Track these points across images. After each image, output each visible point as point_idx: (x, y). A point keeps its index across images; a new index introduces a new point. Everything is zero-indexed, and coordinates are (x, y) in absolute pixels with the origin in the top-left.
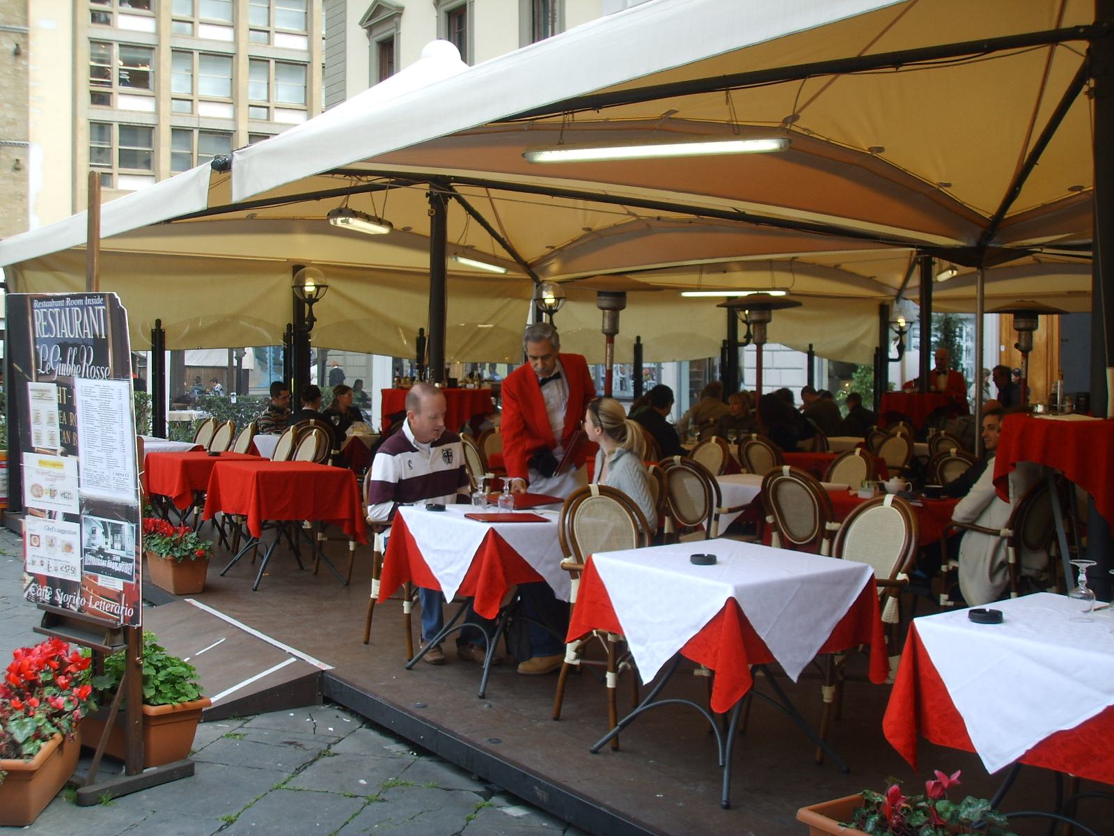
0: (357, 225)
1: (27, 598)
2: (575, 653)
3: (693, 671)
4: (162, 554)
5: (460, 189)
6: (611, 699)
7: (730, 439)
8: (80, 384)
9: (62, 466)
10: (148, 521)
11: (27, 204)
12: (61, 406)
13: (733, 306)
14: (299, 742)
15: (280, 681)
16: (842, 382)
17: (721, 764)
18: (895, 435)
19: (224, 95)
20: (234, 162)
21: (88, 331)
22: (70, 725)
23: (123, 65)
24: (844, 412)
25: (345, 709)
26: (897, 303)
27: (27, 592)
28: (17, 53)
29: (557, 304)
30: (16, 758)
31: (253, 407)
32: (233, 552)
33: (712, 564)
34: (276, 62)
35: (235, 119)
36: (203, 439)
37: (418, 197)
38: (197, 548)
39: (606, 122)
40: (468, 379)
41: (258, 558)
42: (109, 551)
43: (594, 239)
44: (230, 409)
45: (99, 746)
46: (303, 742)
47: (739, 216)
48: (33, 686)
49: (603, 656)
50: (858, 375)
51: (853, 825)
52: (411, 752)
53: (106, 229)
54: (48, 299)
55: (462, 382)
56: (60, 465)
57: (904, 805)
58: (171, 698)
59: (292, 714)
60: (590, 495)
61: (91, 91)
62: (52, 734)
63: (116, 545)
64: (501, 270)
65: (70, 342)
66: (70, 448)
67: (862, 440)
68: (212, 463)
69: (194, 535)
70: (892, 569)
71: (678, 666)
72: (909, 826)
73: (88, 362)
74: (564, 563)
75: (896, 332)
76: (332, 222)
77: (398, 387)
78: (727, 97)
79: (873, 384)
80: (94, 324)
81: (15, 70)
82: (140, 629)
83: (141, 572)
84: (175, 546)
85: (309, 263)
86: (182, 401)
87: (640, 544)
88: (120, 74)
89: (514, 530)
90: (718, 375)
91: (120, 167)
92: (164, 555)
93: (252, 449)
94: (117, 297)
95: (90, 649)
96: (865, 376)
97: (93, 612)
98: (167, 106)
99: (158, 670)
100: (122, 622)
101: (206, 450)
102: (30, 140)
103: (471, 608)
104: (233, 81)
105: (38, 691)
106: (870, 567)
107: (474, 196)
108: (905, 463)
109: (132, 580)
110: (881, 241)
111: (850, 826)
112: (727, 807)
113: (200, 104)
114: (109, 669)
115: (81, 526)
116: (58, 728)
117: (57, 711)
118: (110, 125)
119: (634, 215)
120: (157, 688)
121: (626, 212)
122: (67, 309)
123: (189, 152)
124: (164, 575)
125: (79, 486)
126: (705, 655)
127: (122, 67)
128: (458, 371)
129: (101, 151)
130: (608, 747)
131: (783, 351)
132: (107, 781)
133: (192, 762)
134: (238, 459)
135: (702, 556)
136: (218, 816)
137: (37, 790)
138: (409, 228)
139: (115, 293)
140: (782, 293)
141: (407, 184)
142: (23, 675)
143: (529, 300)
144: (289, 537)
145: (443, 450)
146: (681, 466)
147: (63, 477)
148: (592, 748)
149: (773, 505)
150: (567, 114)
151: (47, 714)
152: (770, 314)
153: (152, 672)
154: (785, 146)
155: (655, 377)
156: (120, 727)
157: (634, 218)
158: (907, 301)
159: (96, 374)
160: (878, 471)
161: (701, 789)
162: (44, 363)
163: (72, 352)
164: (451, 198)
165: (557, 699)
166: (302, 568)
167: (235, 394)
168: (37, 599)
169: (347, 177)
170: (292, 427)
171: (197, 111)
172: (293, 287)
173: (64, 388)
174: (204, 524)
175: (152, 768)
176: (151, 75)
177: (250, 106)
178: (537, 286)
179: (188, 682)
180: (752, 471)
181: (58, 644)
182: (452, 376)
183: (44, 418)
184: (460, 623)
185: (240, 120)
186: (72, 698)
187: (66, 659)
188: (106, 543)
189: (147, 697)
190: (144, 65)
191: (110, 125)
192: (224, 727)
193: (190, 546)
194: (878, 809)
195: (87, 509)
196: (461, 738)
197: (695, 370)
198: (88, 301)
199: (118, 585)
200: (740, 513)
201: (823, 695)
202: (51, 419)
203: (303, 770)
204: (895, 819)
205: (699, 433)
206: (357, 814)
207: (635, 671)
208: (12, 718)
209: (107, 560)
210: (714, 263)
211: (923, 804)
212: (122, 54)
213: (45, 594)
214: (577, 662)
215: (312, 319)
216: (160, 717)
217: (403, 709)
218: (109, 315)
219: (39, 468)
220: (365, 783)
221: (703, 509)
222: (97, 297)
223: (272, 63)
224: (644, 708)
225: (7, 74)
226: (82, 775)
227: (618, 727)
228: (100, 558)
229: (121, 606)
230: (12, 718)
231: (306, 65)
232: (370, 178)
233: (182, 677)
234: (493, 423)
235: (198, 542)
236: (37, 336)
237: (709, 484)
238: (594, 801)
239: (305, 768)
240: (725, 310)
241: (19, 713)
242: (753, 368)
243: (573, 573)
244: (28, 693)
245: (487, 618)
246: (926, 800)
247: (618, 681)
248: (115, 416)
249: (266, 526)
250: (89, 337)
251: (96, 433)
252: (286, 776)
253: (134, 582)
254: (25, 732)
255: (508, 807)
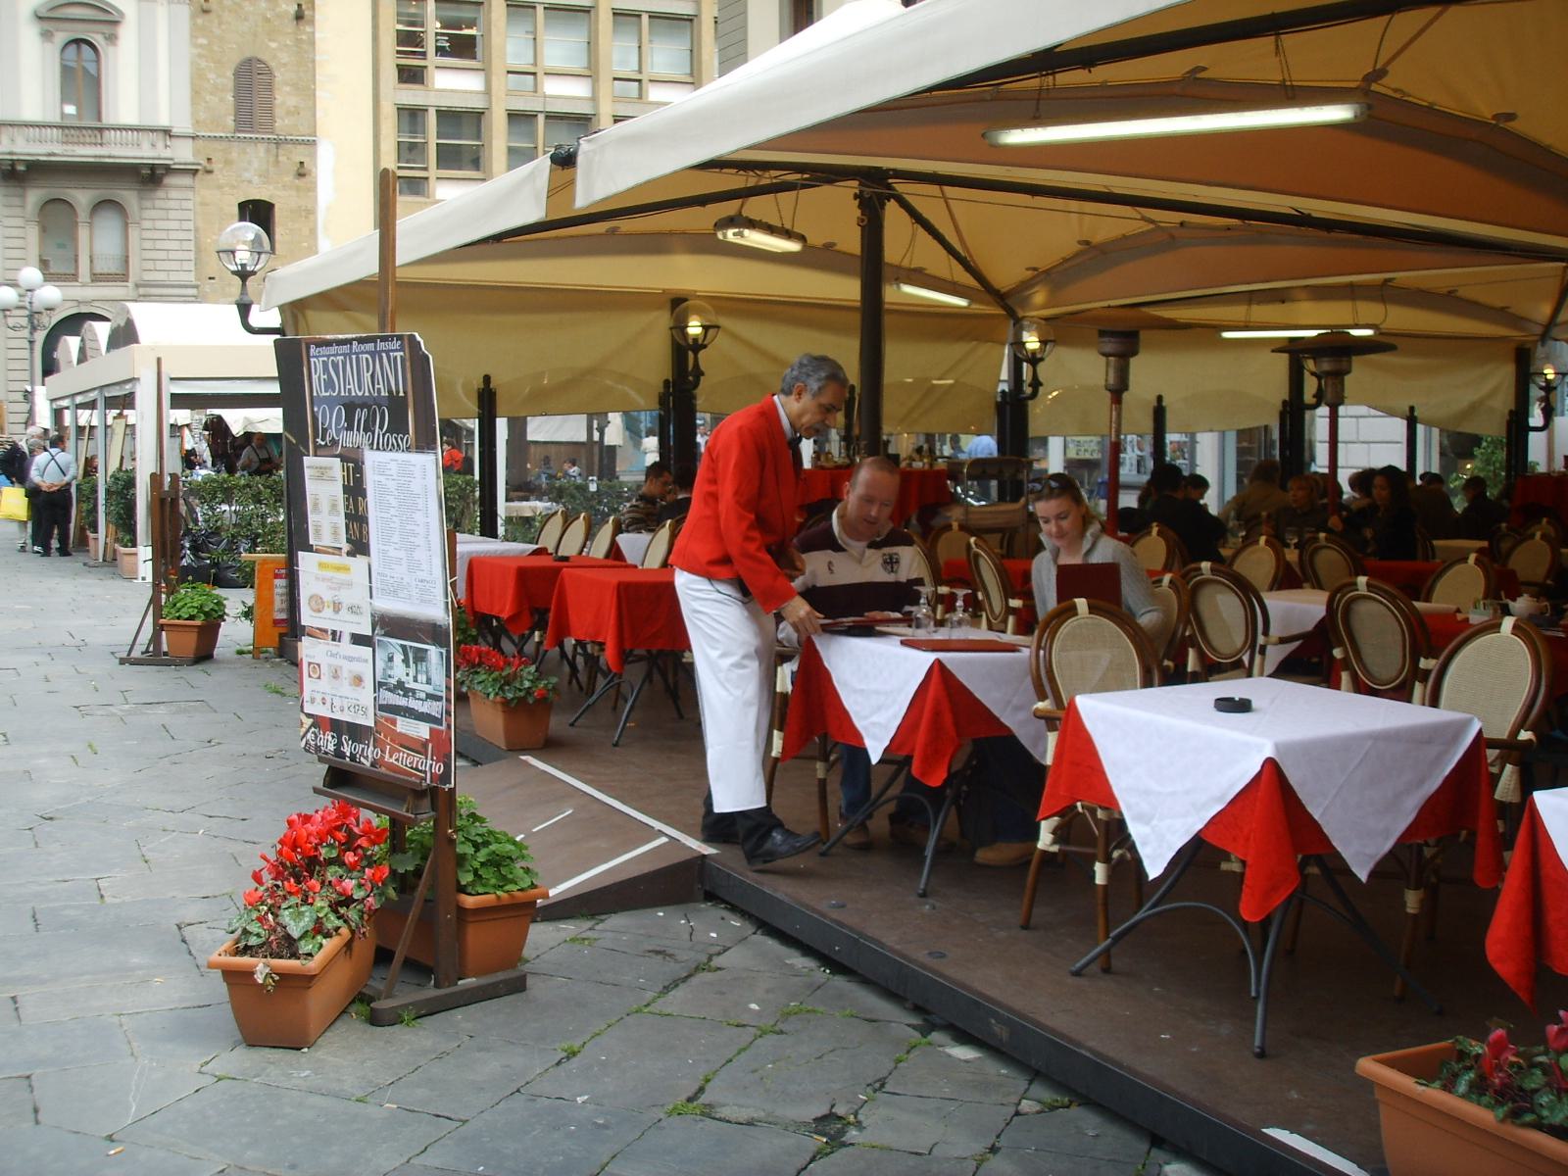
0: (755, 238)
1: (304, 748)
2: (1051, 836)
3: (1220, 864)
4: (488, 694)
5: (901, 187)
6: (1100, 901)
7: (1289, 541)
8: (372, 459)
9: (349, 569)
10: (471, 650)
11: (315, 222)
12: (346, 489)
13: (1295, 351)
14: (670, 951)
15: (647, 868)
16: (1460, 462)
17: (1253, 994)
18: (1532, 536)
19: (578, 64)
20: (580, 153)
21: (381, 386)
22: (361, 918)
23: (442, 28)
24: (1459, 504)
25: (734, 908)
26: (1543, 345)
27: (304, 740)
28: (299, 17)
29: (1042, 349)
30: (290, 958)
31: (620, 495)
32: (587, 694)
33: (1248, 711)
34: (650, 17)
35: (594, 99)
36: (548, 540)
37: (842, 198)
38: (537, 687)
39: (1103, 86)
40: (915, 455)
41: (621, 702)
42: (411, 685)
43: (1094, 256)
44: (589, 500)
45: (399, 948)
46: (676, 952)
47: (1302, 220)
48: (312, 864)
49: (1091, 841)
50: (1483, 451)
51: (1437, 1084)
52: (823, 969)
53: (403, 255)
54: (328, 343)
55: (905, 459)
56: (346, 569)
57: (1513, 1059)
58: (494, 886)
59: (661, 914)
60: (1077, 614)
61: (398, 65)
62: (337, 929)
63: (419, 678)
64: (961, 302)
65: (357, 402)
66: (359, 546)
67: (1485, 544)
68: (559, 570)
69: (533, 668)
70: (1511, 725)
71: (1197, 855)
72: (1521, 1089)
73: (381, 428)
74: (1037, 709)
75: (1541, 388)
76: (720, 236)
77: (816, 467)
78: (1277, 46)
79: (1504, 464)
80: (388, 376)
81: (297, 39)
82: (452, 791)
83: (453, 714)
84: (508, 683)
85: (694, 295)
86: (521, 489)
87: (1147, 683)
88: (437, 41)
89: (969, 662)
90: (1277, 452)
91: (438, 168)
92: (492, 696)
93: (614, 552)
94: (419, 338)
95: (388, 817)
96: (1493, 453)
97: (391, 767)
98: (501, 82)
99: (477, 847)
100: (428, 781)
101: (551, 554)
102: (318, 134)
103: (909, 772)
104: (592, 46)
105: (319, 872)
106: (1476, 720)
107: (924, 198)
108: (1547, 577)
109: (441, 725)
110: (1513, 253)
111: (1433, 1085)
112: (1262, 1055)
113: (650, 84)
114: (413, 845)
115: (374, 651)
116: (345, 921)
117: (343, 898)
118: (424, 110)
119: (1152, 222)
120: (476, 872)
121: (1139, 217)
122: (354, 357)
123: (532, 145)
124: (489, 720)
125: (371, 597)
126: (1235, 839)
127: (439, 31)
128: (903, 443)
129: (412, 147)
130: (1095, 968)
131: (1373, 417)
132: (409, 994)
133: (523, 973)
134: (594, 565)
135: (1231, 700)
136: (557, 1046)
137: (319, 1001)
138: (832, 245)
139: (416, 334)
140: (1368, 332)
141: (830, 182)
142: (299, 850)
143: (1003, 344)
144: (664, 675)
145: (884, 555)
146: (1212, 577)
147: (350, 585)
148: (1073, 969)
149: (1343, 634)
150: (1045, 75)
151: (331, 902)
152: (1350, 362)
153: (469, 850)
154: (1362, 114)
155: (1186, 456)
156: (427, 923)
157: (1152, 226)
158: (1558, 343)
159: (393, 445)
160: (1501, 587)
161: (1225, 1029)
162: (325, 431)
163: (361, 415)
164: (889, 201)
165: (1026, 901)
166: (681, 717)
167: (595, 478)
168: (318, 748)
169: (741, 172)
170: (669, 522)
171: (542, 89)
172: (671, 329)
173: (351, 465)
174: (547, 656)
175: (470, 980)
176: (479, 41)
177: (615, 79)
178: (1014, 325)
179: (518, 866)
180: (1318, 585)
181: (345, 810)
182: (891, 450)
183: (325, 506)
184: (895, 790)
185: (601, 100)
186: (363, 881)
187: (356, 830)
188: (407, 675)
189: (463, 883)
190: (470, 27)
191: (424, 110)
192: (569, 928)
193: (527, 684)
194: (1476, 1062)
195: (382, 628)
196: (892, 950)
197: (1245, 444)
198: (381, 345)
199: (423, 731)
200: (1297, 644)
201: (1405, 903)
202: (334, 506)
203: (673, 988)
204: (1498, 1077)
205: (1244, 533)
206: (744, 1049)
207: (1137, 862)
208: (284, 906)
209: (408, 697)
210: (1269, 289)
211: (1542, 1059)
212: (440, 13)
213: (328, 743)
214: (1055, 848)
215: (698, 373)
216: (481, 912)
217: (814, 910)
218: (408, 364)
219: (320, 572)
220: (757, 1008)
221: (1243, 638)
222: (393, 340)
223: (645, 18)
224: (1151, 912)
225: (286, 45)
226: (377, 985)
227: (1109, 940)
228: (399, 694)
229: (426, 759)
230: (284, 906)
231: (691, 20)
232: (774, 173)
233: (510, 858)
234: (950, 517)
235: (537, 679)
236: (315, 394)
237: (1252, 602)
238: (1071, 1040)
239: (677, 986)
240: (1285, 356)
241: (294, 900)
242: (1325, 442)
243: (1050, 722)
244: (305, 873)
245: (930, 784)
246: (1546, 1053)
247: (1112, 875)
248: (418, 501)
249: (630, 659)
250: (383, 394)
251: (392, 525)
252: (649, 995)
253: (443, 728)
254: (302, 924)
255: (953, 1047)
